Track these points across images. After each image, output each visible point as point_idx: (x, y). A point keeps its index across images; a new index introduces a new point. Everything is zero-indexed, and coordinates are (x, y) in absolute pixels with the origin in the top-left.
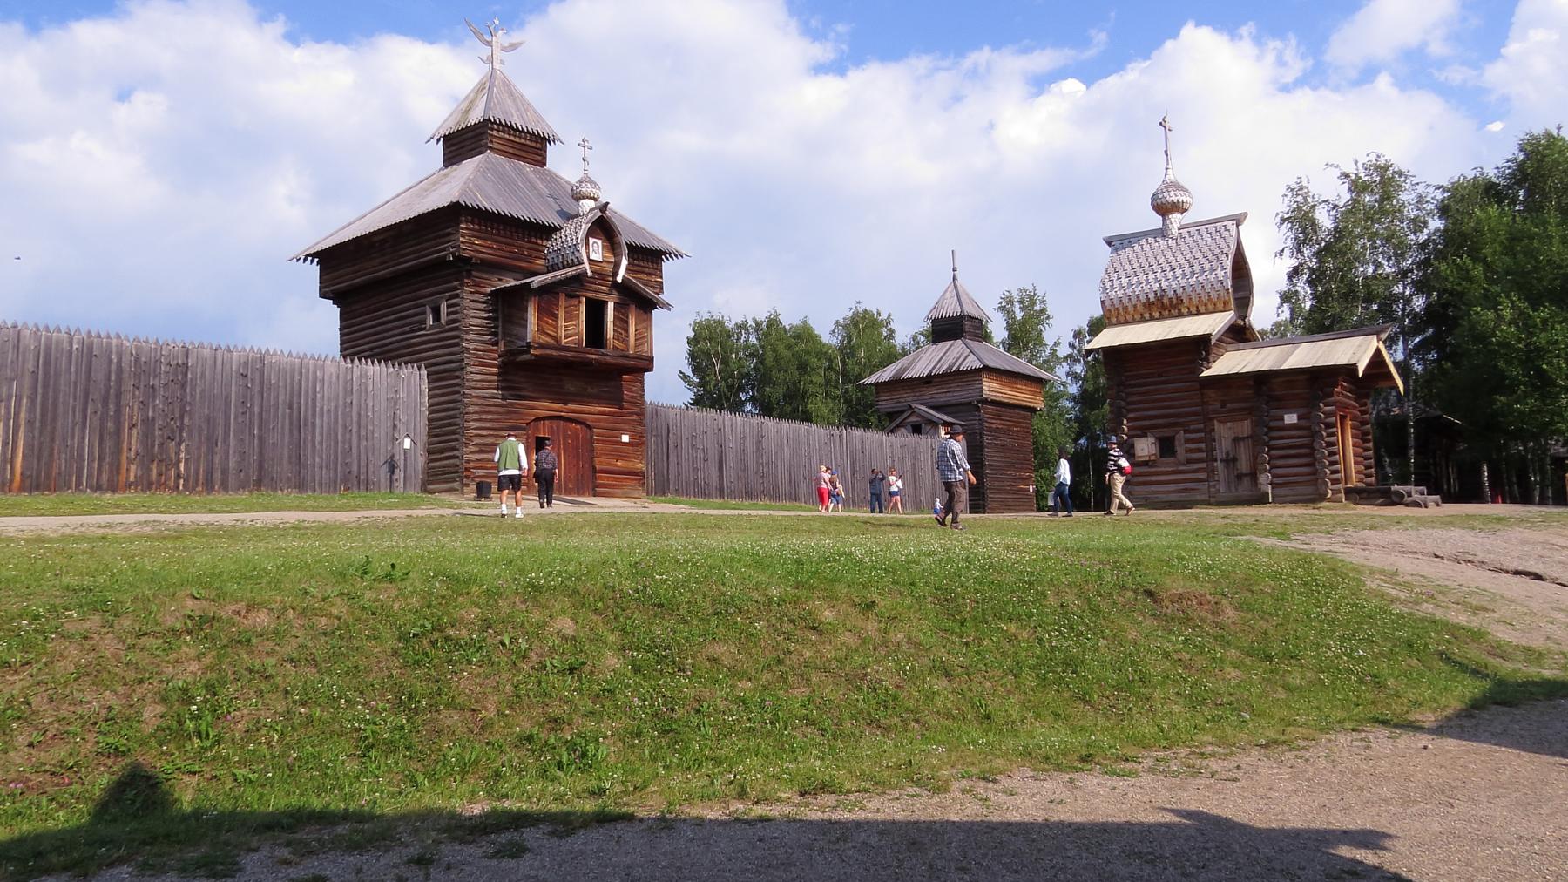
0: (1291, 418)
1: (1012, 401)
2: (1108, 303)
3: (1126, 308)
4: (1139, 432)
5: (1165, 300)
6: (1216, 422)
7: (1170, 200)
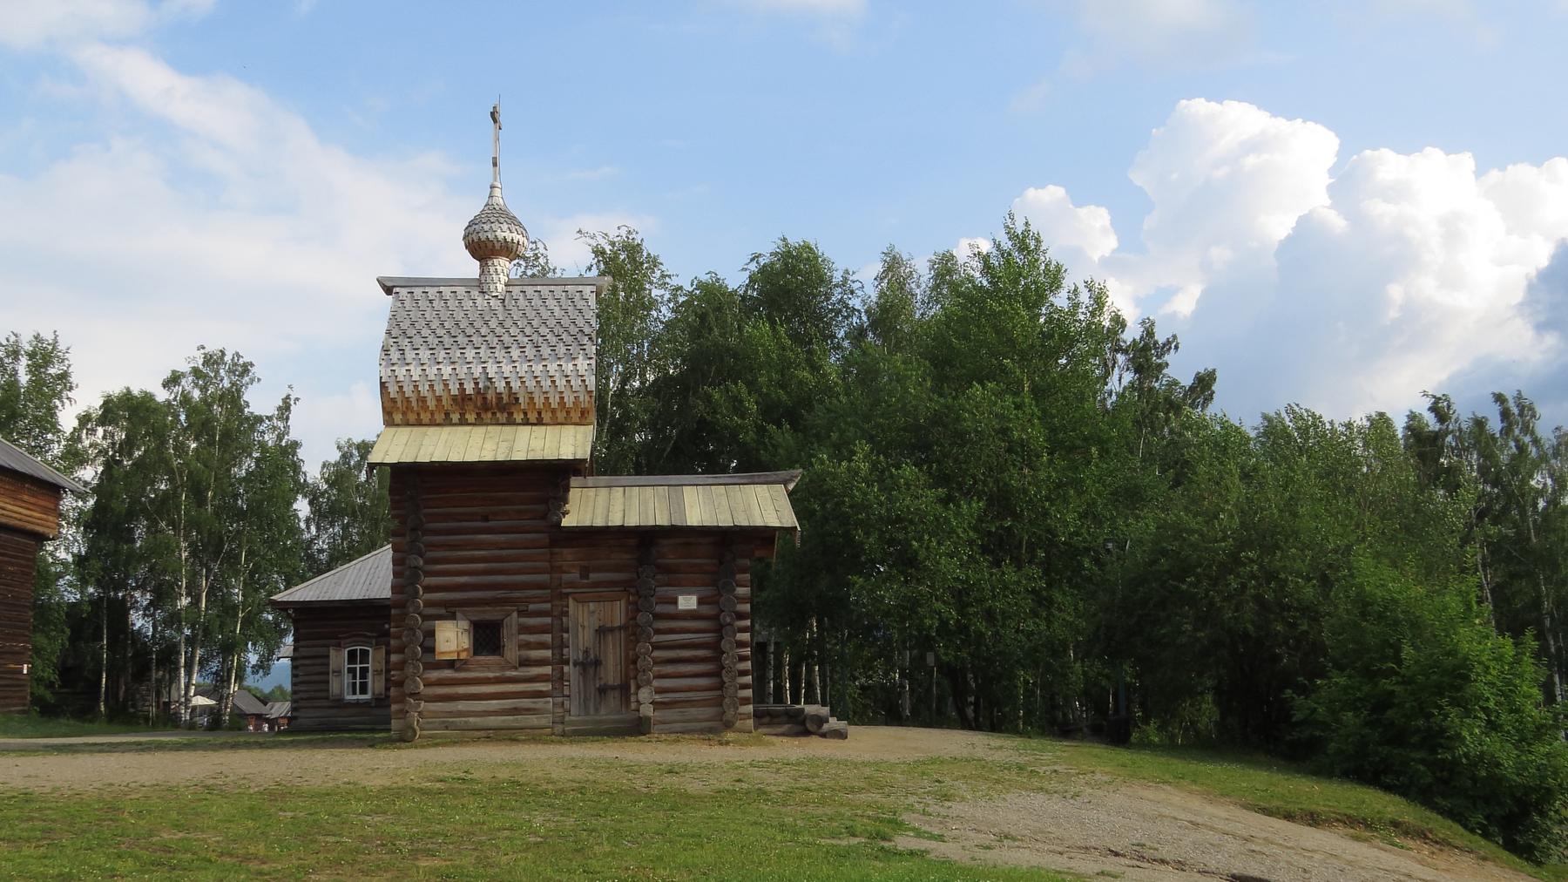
0: (688, 602)
1: (30, 527)
2: (393, 390)
3: (422, 400)
4: (443, 611)
5: (490, 395)
6: (571, 601)
7: (500, 235)
